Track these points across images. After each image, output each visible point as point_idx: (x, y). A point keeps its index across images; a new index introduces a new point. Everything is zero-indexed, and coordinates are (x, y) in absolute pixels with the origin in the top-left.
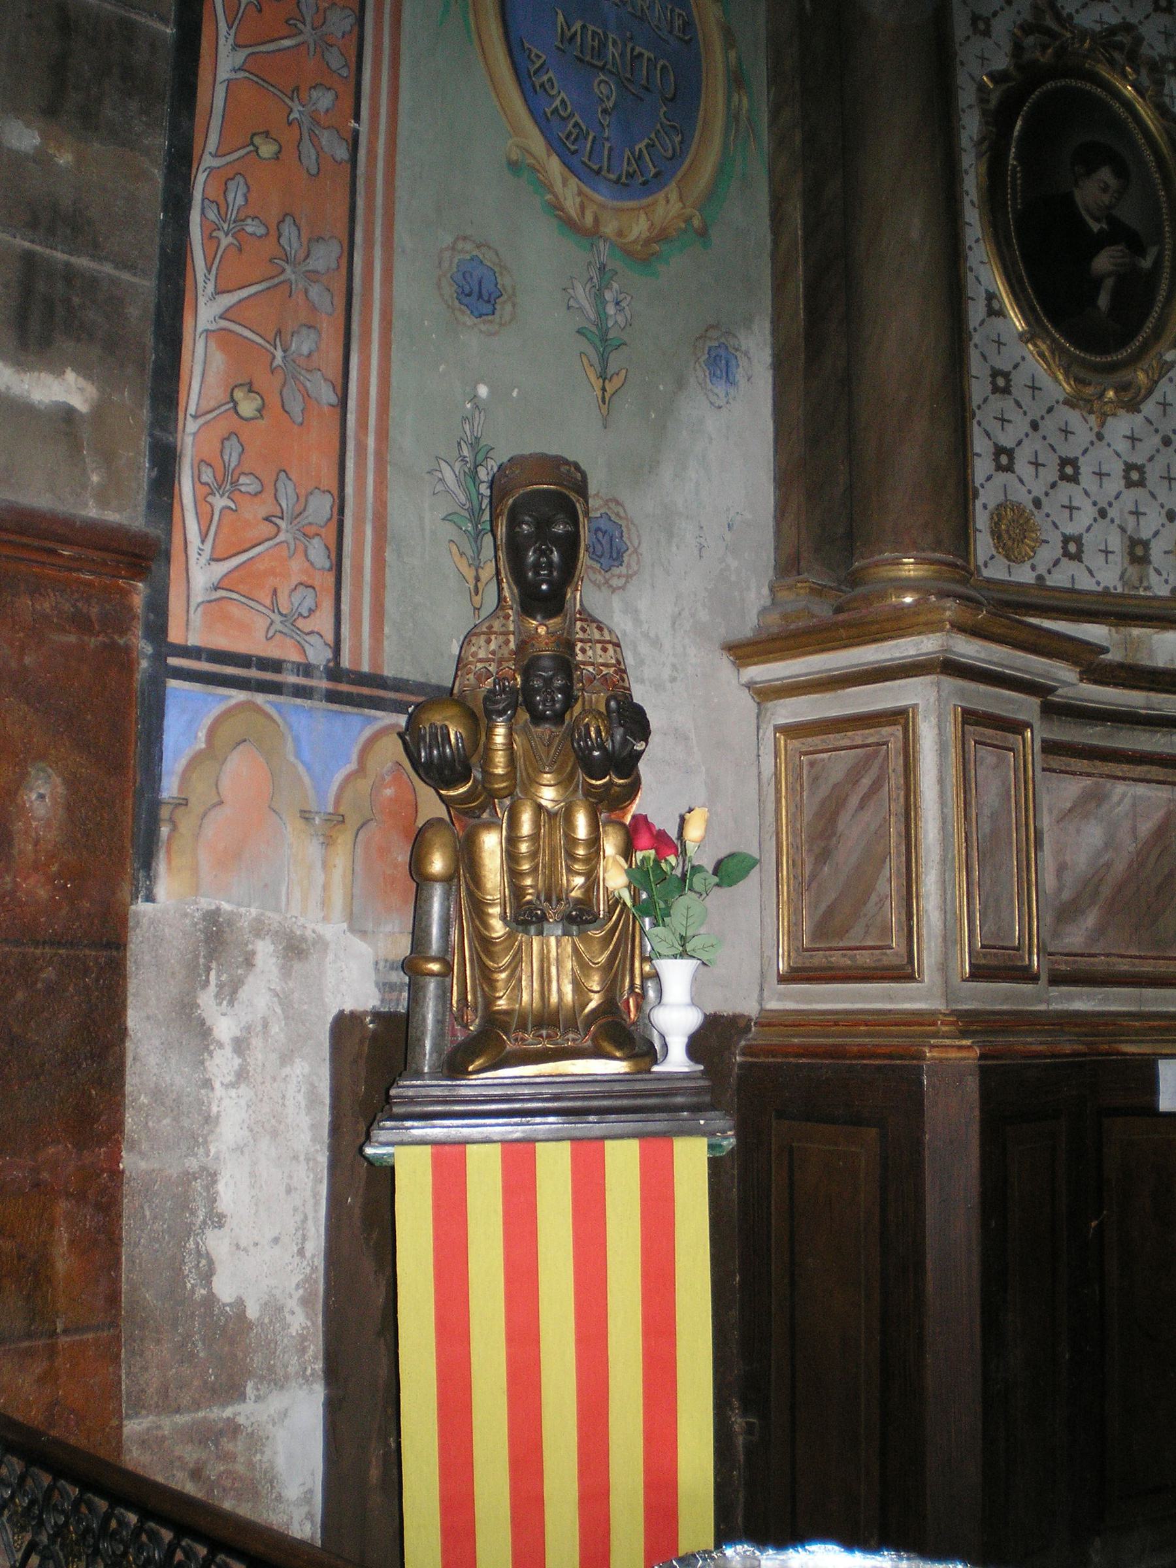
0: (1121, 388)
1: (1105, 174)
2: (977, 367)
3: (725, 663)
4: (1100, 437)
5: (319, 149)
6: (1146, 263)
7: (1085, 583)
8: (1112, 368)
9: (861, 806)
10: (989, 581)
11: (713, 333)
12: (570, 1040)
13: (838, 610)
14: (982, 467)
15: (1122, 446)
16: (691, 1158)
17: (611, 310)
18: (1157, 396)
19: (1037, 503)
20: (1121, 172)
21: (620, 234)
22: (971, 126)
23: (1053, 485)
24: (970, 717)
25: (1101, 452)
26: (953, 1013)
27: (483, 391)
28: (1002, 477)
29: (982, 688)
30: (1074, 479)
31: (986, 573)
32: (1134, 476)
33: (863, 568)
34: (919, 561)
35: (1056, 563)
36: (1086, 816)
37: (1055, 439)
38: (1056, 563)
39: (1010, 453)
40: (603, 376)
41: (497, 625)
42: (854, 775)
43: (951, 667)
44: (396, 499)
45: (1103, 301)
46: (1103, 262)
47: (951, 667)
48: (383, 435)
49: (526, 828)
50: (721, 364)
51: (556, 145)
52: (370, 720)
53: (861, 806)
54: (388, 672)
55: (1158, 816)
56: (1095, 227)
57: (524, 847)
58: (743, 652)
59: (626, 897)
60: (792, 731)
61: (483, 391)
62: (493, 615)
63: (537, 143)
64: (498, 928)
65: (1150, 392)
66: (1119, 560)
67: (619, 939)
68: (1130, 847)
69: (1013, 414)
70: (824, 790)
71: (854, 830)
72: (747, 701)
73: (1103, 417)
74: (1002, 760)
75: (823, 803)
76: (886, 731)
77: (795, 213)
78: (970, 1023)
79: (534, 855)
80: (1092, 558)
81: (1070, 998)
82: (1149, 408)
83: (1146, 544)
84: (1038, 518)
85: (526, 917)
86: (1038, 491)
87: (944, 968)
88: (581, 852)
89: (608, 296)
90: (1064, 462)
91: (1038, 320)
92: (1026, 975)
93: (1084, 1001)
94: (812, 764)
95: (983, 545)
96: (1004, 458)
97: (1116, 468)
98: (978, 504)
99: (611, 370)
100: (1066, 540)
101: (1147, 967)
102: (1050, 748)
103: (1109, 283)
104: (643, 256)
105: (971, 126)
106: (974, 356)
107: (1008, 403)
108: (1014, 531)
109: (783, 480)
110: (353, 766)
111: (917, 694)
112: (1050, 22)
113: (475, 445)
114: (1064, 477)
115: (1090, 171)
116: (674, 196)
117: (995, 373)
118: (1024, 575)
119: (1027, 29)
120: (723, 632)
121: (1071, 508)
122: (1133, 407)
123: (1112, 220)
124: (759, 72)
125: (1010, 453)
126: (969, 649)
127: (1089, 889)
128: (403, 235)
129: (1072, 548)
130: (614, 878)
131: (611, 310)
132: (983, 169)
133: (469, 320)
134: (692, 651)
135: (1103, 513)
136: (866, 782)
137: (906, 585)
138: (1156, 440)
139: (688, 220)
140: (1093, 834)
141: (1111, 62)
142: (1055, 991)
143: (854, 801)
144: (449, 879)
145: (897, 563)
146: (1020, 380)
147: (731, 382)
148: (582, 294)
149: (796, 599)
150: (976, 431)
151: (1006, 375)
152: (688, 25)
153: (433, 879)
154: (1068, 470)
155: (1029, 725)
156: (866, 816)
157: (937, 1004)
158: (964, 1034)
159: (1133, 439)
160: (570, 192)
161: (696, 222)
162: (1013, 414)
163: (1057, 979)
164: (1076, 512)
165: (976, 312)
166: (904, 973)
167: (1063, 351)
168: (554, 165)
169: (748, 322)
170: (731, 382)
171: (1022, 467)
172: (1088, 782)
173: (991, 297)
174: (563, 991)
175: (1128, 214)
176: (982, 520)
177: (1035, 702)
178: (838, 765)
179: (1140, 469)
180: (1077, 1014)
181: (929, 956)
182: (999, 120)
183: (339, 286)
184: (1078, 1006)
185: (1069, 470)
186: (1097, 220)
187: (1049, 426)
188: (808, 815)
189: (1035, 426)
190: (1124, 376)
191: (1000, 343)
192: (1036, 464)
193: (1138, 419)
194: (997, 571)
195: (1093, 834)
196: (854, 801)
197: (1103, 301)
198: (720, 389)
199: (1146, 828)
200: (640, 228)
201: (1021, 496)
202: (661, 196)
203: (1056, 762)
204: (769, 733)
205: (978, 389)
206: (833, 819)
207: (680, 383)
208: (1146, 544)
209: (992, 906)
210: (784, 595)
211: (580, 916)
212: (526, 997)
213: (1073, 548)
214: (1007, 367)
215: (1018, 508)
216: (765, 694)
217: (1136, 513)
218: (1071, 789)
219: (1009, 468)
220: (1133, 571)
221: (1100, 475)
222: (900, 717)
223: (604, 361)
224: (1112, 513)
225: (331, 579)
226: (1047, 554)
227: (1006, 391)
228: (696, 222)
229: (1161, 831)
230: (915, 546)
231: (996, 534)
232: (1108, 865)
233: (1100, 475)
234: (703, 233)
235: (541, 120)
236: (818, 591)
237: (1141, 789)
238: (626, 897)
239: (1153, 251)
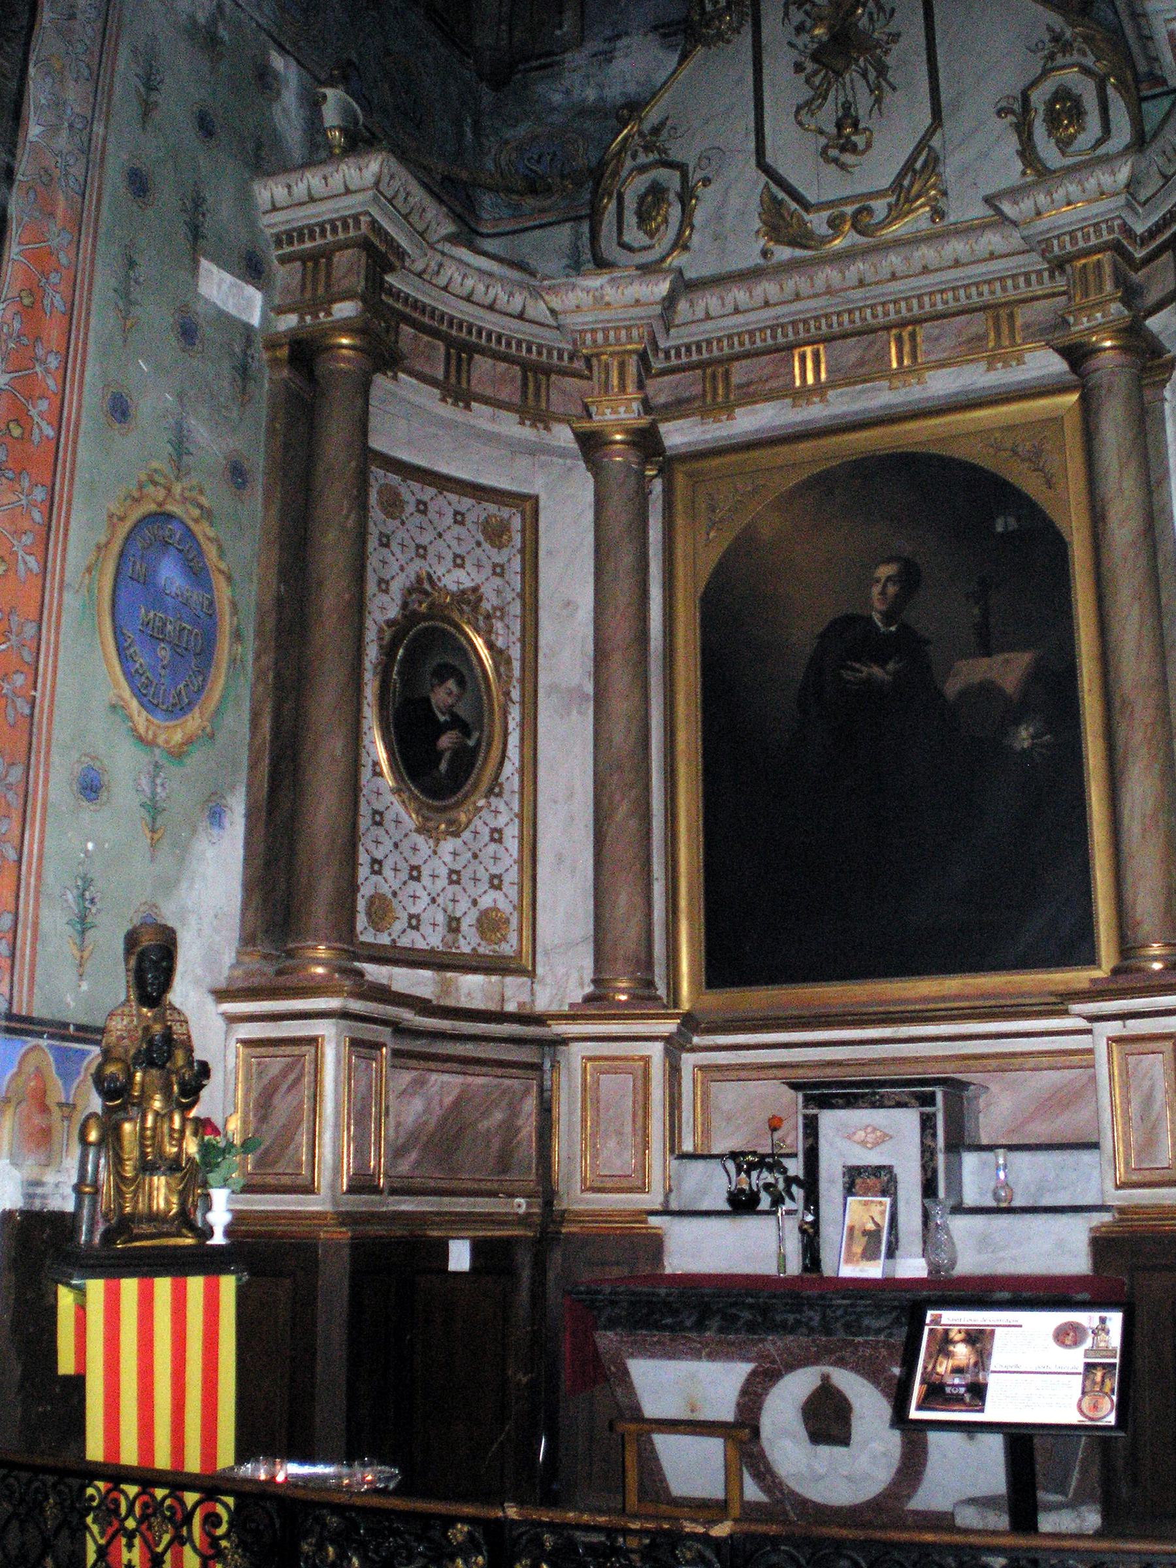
0: (450, 823)
1: (451, 684)
2: (364, 809)
3: (209, 1000)
4: (435, 852)
5: (15, 708)
6: (471, 743)
7: (421, 944)
8: (445, 809)
9: (289, 1089)
10: (362, 943)
11: (214, 798)
12: (166, 1228)
13: (280, 973)
14: (363, 872)
15: (448, 858)
16: (228, 1285)
17: (159, 790)
18: (472, 827)
19: (395, 894)
20: (461, 683)
21: (167, 742)
22: (372, 653)
23: (405, 883)
24: (355, 1042)
25: (435, 862)
26: (340, 1214)
27: (90, 846)
28: (375, 878)
29: (360, 1024)
30: (418, 879)
31: (362, 938)
32: (454, 877)
33: (298, 948)
34: (328, 948)
35: (404, 931)
36: (412, 1095)
37: (408, 853)
38: (404, 931)
39: (380, 863)
40: (153, 831)
41: (126, 1010)
42: (284, 1073)
43: (344, 1015)
44: (44, 912)
45: (443, 766)
46: (446, 741)
47: (344, 1015)
48: (39, 877)
49: (149, 1123)
50: (216, 816)
51: (138, 693)
52: (25, 1042)
53: (289, 1089)
54: (34, 1015)
55: (455, 1093)
56: (442, 718)
57: (149, 1133)
58: (221, 995)
59: (197, 1157)
60: (247, 1043)
61: (90, 846)
62: (123, 1004)
63: (127, 693)
64: (129, 1172)
65: (467, 826)
66: (441, 930)
67: (193, 1179)
68: (438, 1111)
69: (384, 838)
70: (266, 1081)
71: (282, 1106)
72: (221, 1023)
73: (438, 841)
74: (369, 1066)
75: (265, 1088)
76: (305, 1048)
77: (266, 723)
78: (346, 1218)
79: (153, 1137)
80: (426, 928)
81: (399, 1203)
82: (467, 835)
83: (458, 920)
84: (395, 902)
85: (147, 1167)
86: (395, 887)
87: (333, 1186)
88: (176, 1135)
89: (159, 781)
90: (413, 868)
91: (403, 780)
92: (376, 1190)
93: (408, 1205)
94: (259, 1064)
95: (361, 921)
96: (377, 866)
97: (443, 872)
98: (359, 896)
99: (158, 824)
100: (411, 917)
101: (444, 1184)
102: (396, 1053)
103: (447, 755)
104: (178, 754)
105: (372, 653)
106: (363, 801)
107: (380, 832)
108: (380, 911)
109: (249, 887)
110: (15, 1070)
111: (324, 1029)
112: (427, 586)
113: (84, 879)
114: (412, 878)
115: (443, 681)
116: (197, 715)
117: (375, 812)
118: (384, 939)
119: (410, 591)
120: (209, 982)
121: (414, 897)
122: (456, 834)
123: (454, 716)
124: (249, 632)
125: (380, 863)
126: (356, 1006)
127: (413, 1137)
128: (55, 758)
129: (414, 922)
130: (191, 1147)
131: (159, 790)
132: (377, 683)
133: (85, 803)
134: (192, 994)
135: (434, 900)
136: (292, 1077)
137: (318, 962)
138: (469, 855)
139: (204, 729)
140: (418, 1104)
141: (462, 612)
142: (392, 1199)
143: (285, 1086)
144: (100, 1144)
145: (315, 948)
146: (389, 816)
147: (220, 826)
148: (144, 782)
149: (254, 963)
150: (361, 849)
151: (381, 814)
152: (211, 603)
153: (90, 1144)
154: (415, 874)
155: (384, 1045)
156: (289, 1098)
157: (327, 1207)
158: (342, 1224)
159: (455, 854)
160: (141, 718)
161: (208, 730)
162: (384, 838)
163: (394, 1192)
164: (418, 900)
165: (366, 774)
166: (309, 1189)
167: (416, 798)
168: (134, 704)
169: (233, 787)
170: (220, 826)
171: (387, 872)
172: (414, 1073)
173: (376, 764)
174: (159, 1203)
175: (462, 711)
176: (361, 905)
177: (389, 1030)
178: (276, 1066)
179: (458, 873)
180: (403, 1212)
181: (323, 1179)
182: (388, 651)
183: (21, 793)
184: (404, 1208)
185: (415, 873)
186: (443, 714)
187: (405, 846)
188: (254, 1095)
189: (396, 845)
190: (452, 815)
191: (379, 794)
192: (395, 870)
193: (459, 841)
194: (367, 937)
195: (418, 1104)
196: (285, 1086)
197: (443, 766)
198: (215, 832)
199: (448, 1100)
200: (178, 737)
201: (385, 890)
202: (189, 717)
203: (398, 1062)
204: (233, 1042)
205: (364, 822)
206: (271, 1096)
207: (194, 831)
208: (458, 920)
209: (361, 1153)
210: (247, 959)
211: (174, 1166)
212: (140, 1206)
213: (415, 922)
214: (382, 809)
215: (383, 897)
216: (233, 1019)
217: (454, 901)
218: (406, 1077)
219: (379, 873)
220: (450, 937)
221: (433, 876)
222: (313, 1041)
223: (154, 819)
224: (440, 900)
225: (9, 962)
226: (398, 926)
227: (380, 824)
228: (208, 730)
229: (457, 1103)
230: (327, 939)
231: (369, 914)
232: (425, 1123)
233: (433, 876)
234: (212, 736)
235: (128, 675)
236: (265, 957)
237: (446, 1077)
238: (197, 1157)
239: (476, 735)
